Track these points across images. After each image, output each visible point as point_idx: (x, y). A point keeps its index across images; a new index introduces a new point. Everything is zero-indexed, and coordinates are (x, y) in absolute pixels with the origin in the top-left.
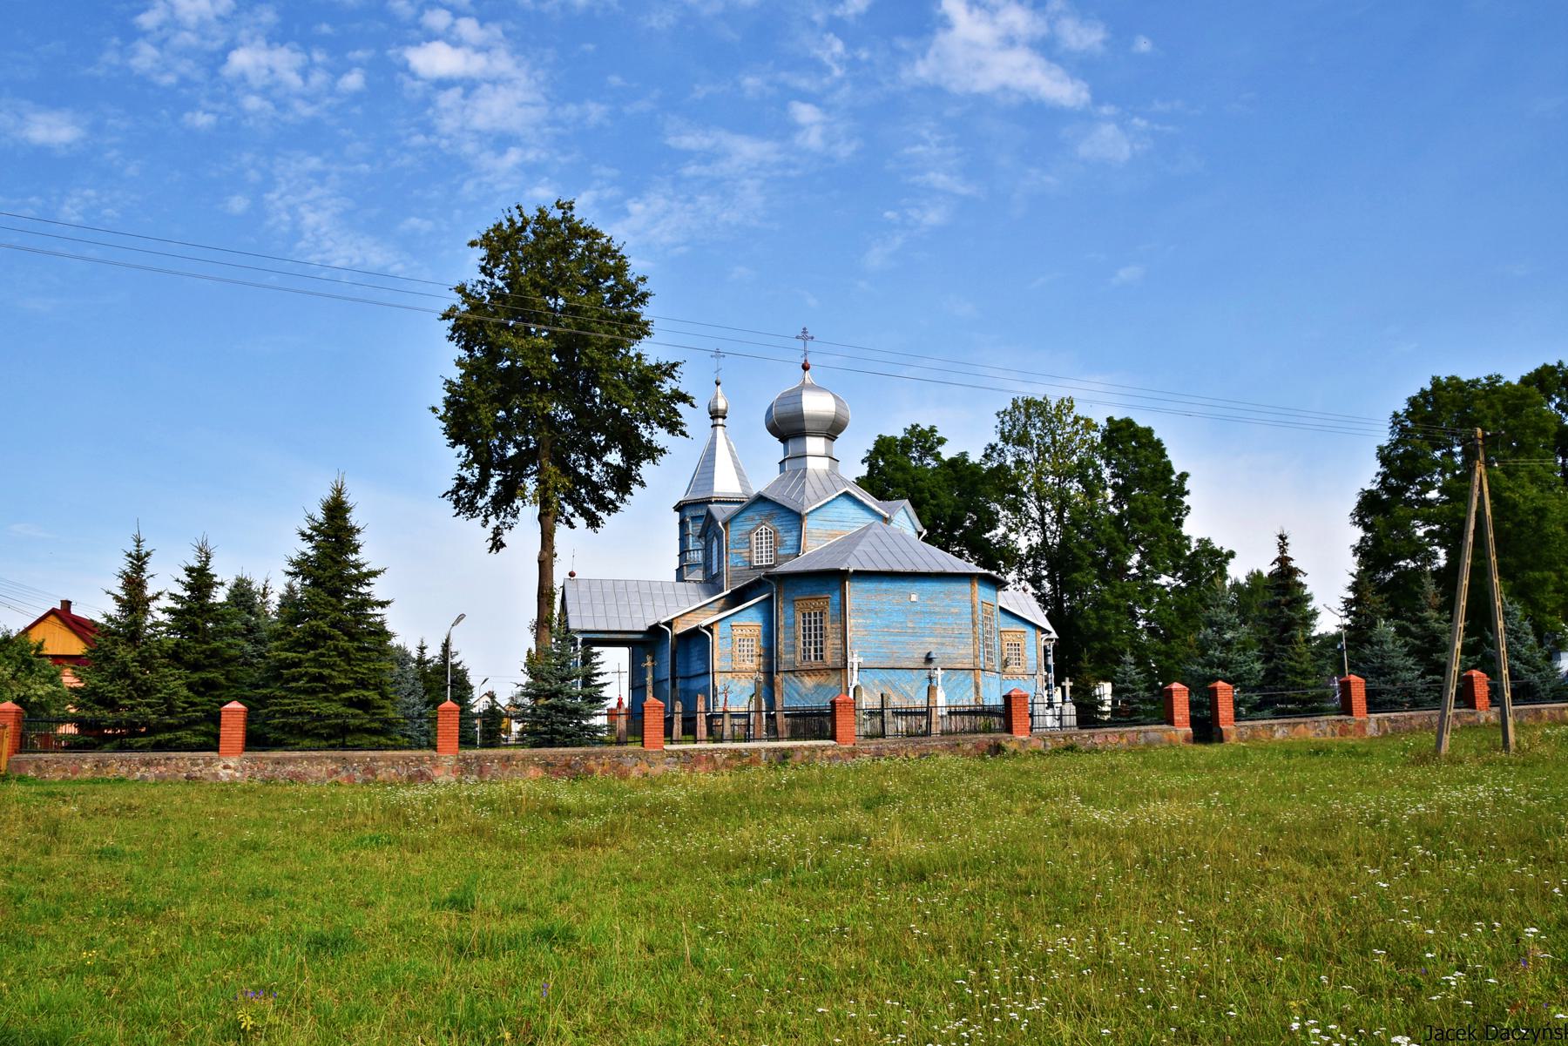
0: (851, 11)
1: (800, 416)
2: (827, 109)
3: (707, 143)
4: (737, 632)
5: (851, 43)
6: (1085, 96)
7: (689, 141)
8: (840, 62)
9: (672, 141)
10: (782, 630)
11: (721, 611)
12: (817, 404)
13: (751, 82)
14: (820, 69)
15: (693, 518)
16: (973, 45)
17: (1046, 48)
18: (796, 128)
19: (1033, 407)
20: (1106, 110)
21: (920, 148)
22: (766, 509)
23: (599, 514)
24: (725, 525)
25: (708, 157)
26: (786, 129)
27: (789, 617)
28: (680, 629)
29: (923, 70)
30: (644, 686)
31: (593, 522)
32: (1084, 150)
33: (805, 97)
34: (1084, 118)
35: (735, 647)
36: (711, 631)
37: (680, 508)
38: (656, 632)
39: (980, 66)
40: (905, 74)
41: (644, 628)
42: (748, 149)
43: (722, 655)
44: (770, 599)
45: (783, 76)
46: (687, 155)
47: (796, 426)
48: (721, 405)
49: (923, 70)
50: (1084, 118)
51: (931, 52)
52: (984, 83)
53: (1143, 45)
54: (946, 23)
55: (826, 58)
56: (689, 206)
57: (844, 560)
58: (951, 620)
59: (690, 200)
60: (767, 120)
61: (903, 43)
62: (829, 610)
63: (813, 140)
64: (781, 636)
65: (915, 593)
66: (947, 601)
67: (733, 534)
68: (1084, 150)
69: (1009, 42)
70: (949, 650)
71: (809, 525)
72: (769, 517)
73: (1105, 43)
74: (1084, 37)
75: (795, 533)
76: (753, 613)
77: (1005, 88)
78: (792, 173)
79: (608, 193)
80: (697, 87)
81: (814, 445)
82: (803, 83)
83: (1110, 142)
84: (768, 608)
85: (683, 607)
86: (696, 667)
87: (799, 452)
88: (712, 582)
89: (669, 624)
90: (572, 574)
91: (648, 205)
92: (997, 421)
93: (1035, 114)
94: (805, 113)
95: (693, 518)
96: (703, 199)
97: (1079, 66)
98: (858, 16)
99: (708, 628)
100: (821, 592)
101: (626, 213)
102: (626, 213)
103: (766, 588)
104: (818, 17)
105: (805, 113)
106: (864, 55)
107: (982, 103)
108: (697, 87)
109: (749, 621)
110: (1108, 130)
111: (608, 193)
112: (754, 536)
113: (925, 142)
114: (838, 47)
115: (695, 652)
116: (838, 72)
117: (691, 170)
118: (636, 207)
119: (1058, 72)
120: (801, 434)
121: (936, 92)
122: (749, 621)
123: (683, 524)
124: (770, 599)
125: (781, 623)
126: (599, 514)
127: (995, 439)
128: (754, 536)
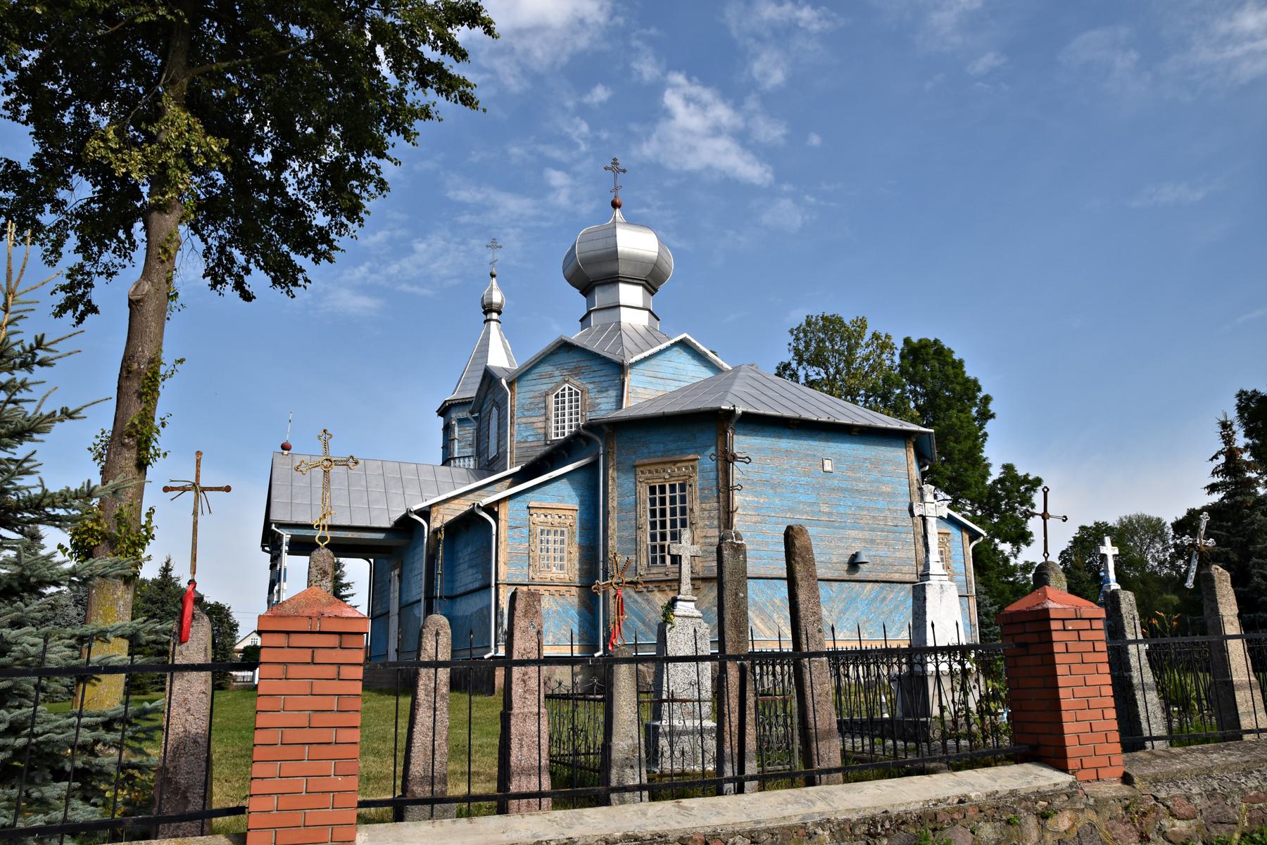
0: (595, 100)
1: (613, 255)
2: (575, 175)
3: (479, 197)
4: (538, 518)
5: (594, 127)
6: (769, 176)
7: (464, 195)
8: (585, 139)
9: (451, 194)
10: (613, 516)
11: (510, 487)
12: (636, 242)
13: (515, 151)
14: (569, 144)
15: (460, 421)
16: (687, 132)
17: (743, 138)
18: (552, 189)
19: (831, 325)
20: (786, 187)
21: (645, 210)
22: (572, 360)
23: (298, 259)
24: (510, 384)
25: (480, 209)
26: (542, 190)
27: (625, 493)
28: (440, 519)
29: (648, 150)
30: (386, 614)
31: (285, 275)
32: (766, 219)
33: (558, 166)
34: (770, 193)
35: (536, 541)
36: (495, 516)
37: (444, 411)
38: (406, 526)
39: (692, 149)
40: (634, 152)
41: (387, 524)
42: (513, 204)
43: (512, 557)
44: (592, 468)
45: (541, 148)
46: (462, 207)
47: (607, 268)
48: (497, 297)
49: (648, 150)
50: (770, 193)
51: (654, 136)
52: (693, 163)
53: (815, 140)
54: (668, 114)
55: (574, 137)
56: (462, 248)
57: (723, 398)
58: (881, 504)
59: (463, 242)
60: (527, 182)
61: (635, 127)
62: (697, 480)
63: (562, 199)
64: (613, 525)
65: (833, 454)
66: (875, 474)
67: (518, 399)
68: (766, 219)
69: (716, 131)
70: (882, 551)
71: (631, 379)
72: (576, 372)
73: (786, 137)
74: (771, 132)
75: (613, 393)
76: (565, 488)
77: (709, 168)
78: (544, 224)
79: (400, 233)
80: (473, 153)
81: (630, 294)
82: (557, 153)
83: (786, 214)
84: (589, 484)
85: (443, 492)
86: (467, 578)
87: (610, 303)
88: (487, 464)
89: (425, 513)
90: (285, 447)
91: (430, 245)
92: (791, 339)
93: (731, 187)
94: (557, 178)
95: (460, 421)
96: (474, 242)
97: (764, 153)
98: (601, 103)
99: (489, 509)
100: (682, 451)
101: (411, 251)
102: (411, 251)
103: (591, 450)
104: (570, 104)
105: (557, 178)
106: (605, 135)
107: (692, 179)
108: (473, 153)
109: (559, 499)
110: (786, 204)
111: (400, 233)
112: (552, 399)
113: (648, 206)
114: (584, 128)
115: (465, 554)
116: (583, 148)
117: (465, 219)
118: (420, 246)
119: (750, 157)
120: (613, 279)
121: (656, 169)
122: (559, 499)
123: (447, 429)
124: (592, 468)
125: (613, 504)
126: (298, 259)
127: (788, 357)
128: (552, 399)
